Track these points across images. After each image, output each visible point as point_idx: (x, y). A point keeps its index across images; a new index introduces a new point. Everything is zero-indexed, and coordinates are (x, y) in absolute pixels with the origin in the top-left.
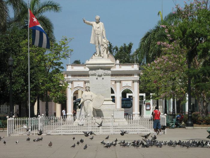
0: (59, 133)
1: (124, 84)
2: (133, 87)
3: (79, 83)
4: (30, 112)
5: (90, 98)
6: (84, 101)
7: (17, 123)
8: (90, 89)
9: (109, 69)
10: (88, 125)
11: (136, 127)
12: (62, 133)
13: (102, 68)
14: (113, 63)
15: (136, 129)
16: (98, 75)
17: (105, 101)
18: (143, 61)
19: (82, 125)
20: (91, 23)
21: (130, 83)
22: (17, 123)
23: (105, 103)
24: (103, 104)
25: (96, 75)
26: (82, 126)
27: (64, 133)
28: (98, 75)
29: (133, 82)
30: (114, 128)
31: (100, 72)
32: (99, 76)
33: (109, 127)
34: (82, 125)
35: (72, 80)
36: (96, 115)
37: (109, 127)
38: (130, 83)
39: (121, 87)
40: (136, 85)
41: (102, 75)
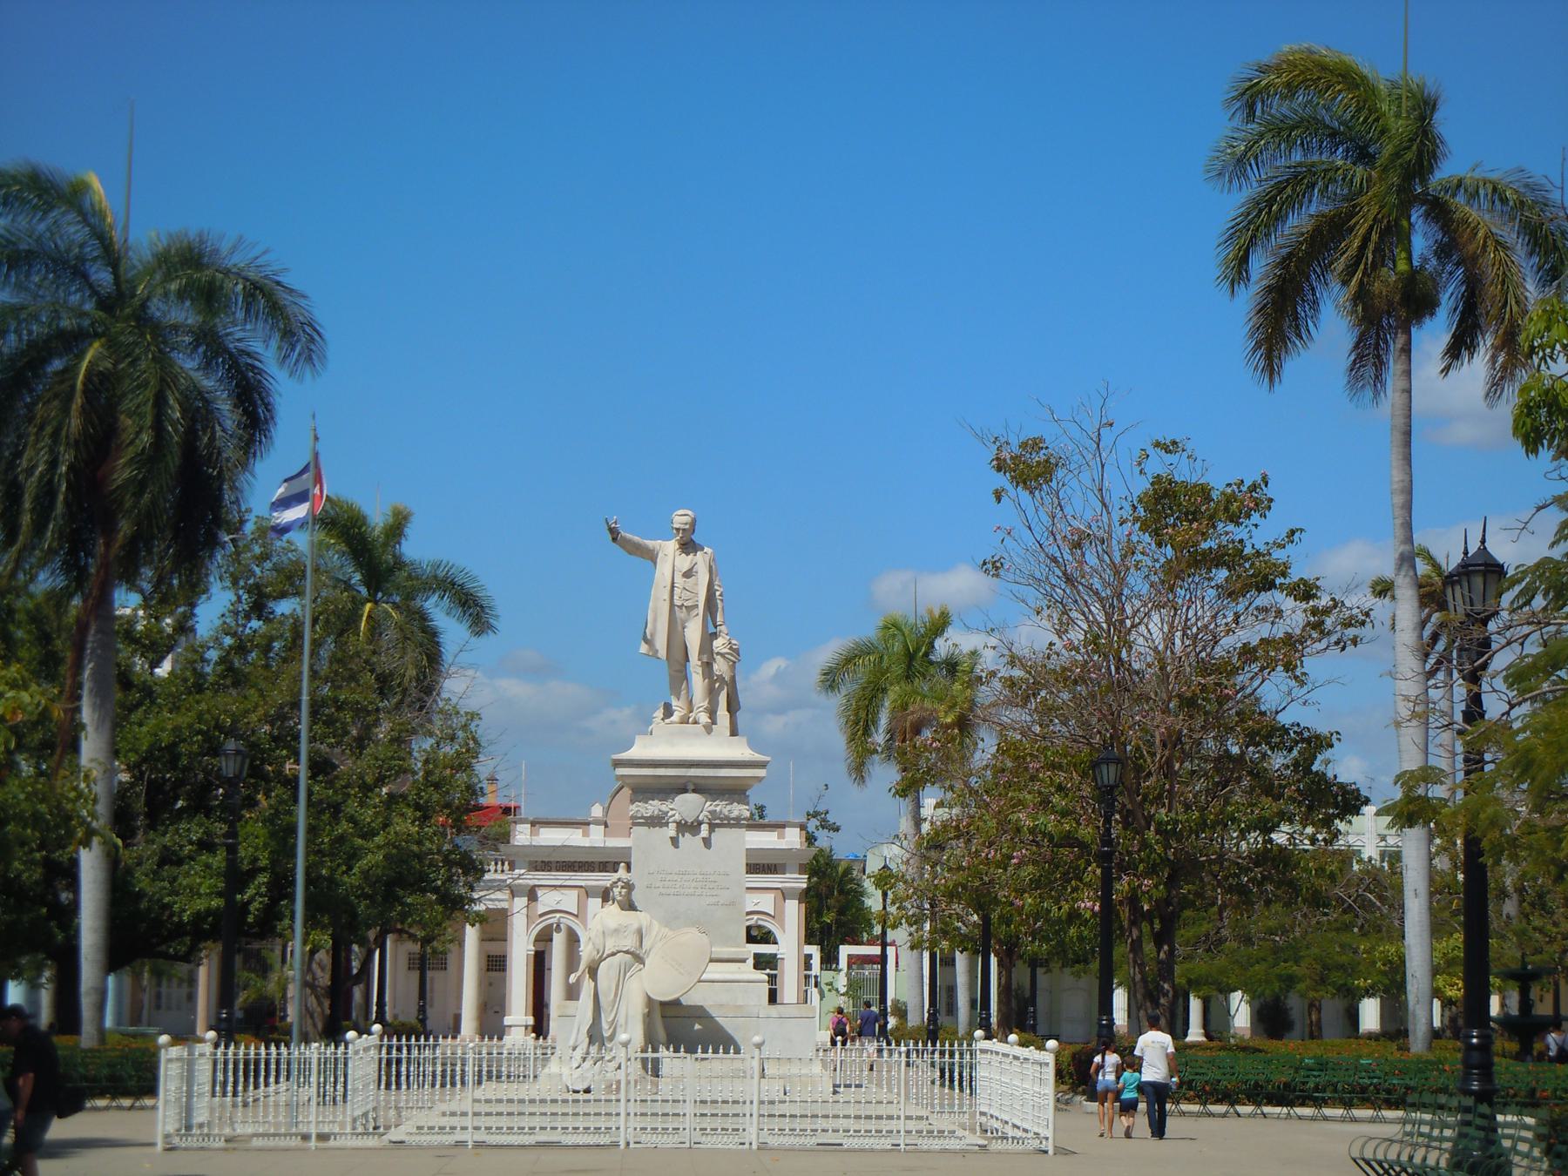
0: (459, 1136)
2: (777, 916)
3: (558, 896)
4: (1000, 1002)
6: (601, 960)
7: (273, 1066)
8: (636, 896)
9: (735, 791)
10: (618, 1089)
11: (882, 1110)
12: (469, 1137)
13: (700, 788)
14: (758, 757)
15: (880, 1113)
16: (679, 824)
17: (712, 961)
18: (1501, 359)
19: (587, 1091)
20: (650, 543)
22: (273, 1066)
23: (716, 971)
24: (704, 977)
25: (667, 824)
26: (587, 1096)
27: (481, 1136)
28: (679, 824)
29: (785, 894)
30: (765, 1110)
31: (687, 805)
32: (683, 827)
33: (738, 1109)
34: (587, 1091)
35: (532, 883)
36: (661, 1034)
37: (738, 1109)
38: (766, 902)
40: (793, 911)
41: (700, 823)
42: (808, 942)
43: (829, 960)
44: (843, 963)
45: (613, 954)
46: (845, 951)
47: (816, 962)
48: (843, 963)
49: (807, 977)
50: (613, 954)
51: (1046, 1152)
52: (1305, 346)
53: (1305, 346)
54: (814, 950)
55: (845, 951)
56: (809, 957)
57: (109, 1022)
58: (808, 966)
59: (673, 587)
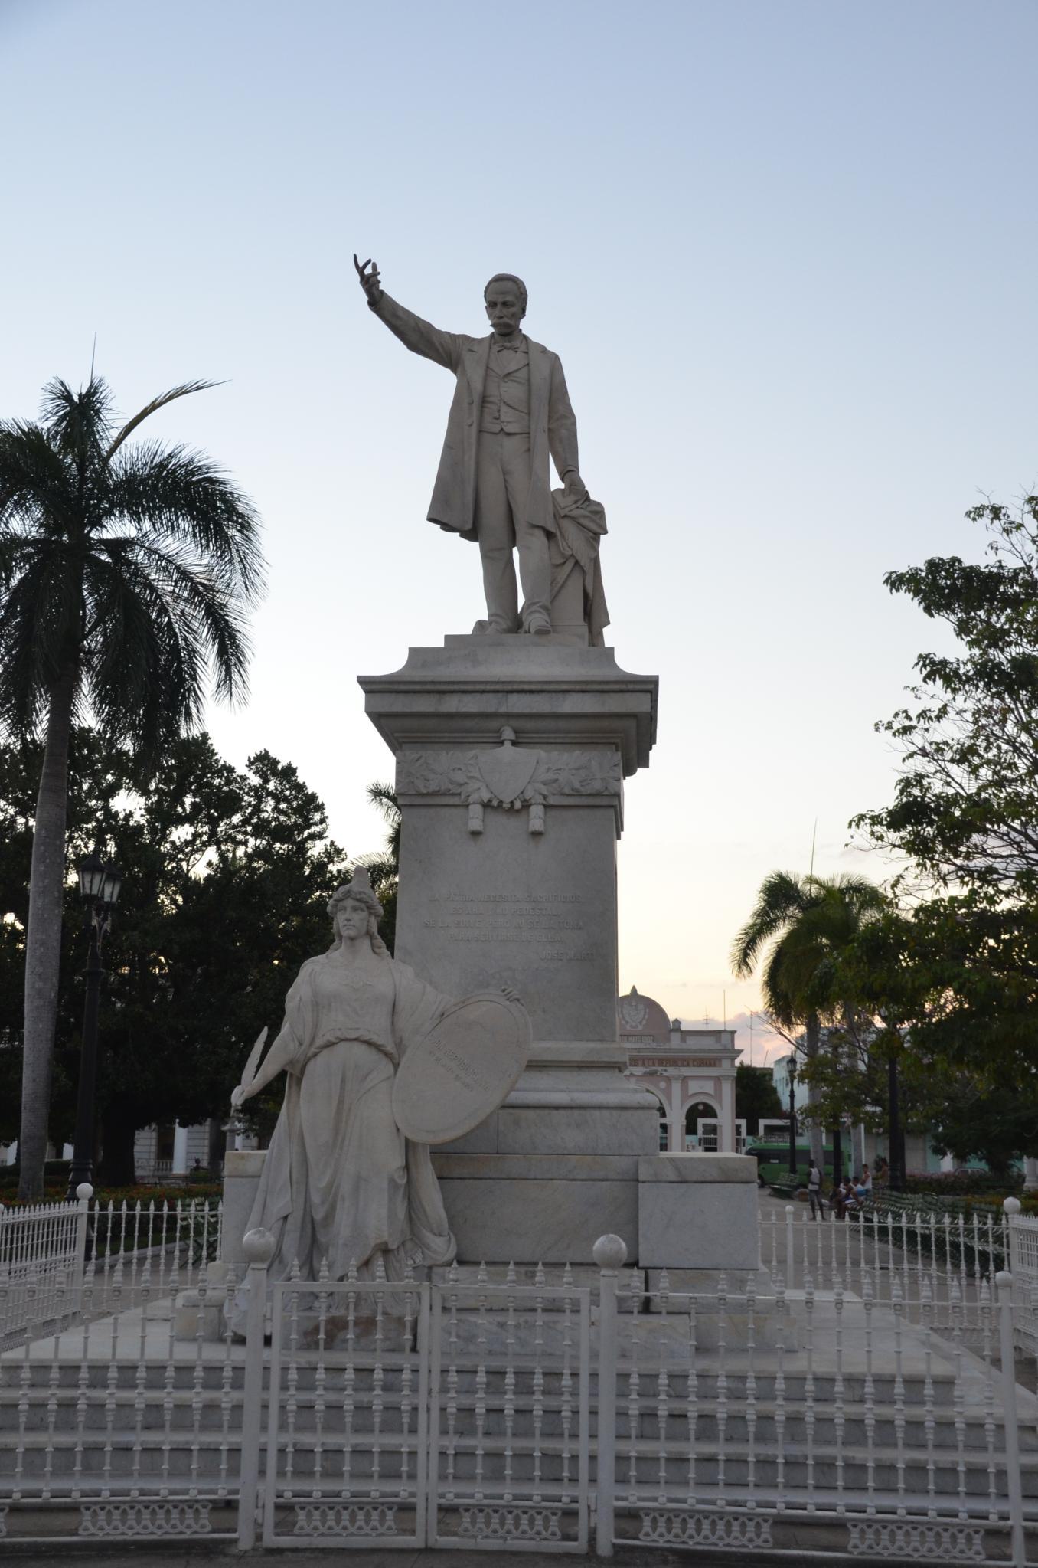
1: (694, 1087)
2: (718, 1095)
5: (376, 1026)
21: (709, 1087)
24: (515, 1097)
38: (709, 1087)
39: (685, 1095)
41: (526, 805)
42: (738, 1116)
43: (752, 1130)
44: (700, 1129)
45: (329, 1045)
46: (762, 1123)
47: (744, 1130)
48: (761, 1131)
49: (738, 1140)
50: (329, 1045)
51: (664, 1147)
52: (263, 598)
53: (263, 598)
54: (743, 1122)
55: (762, 1123)
56: (738, 1127)
57: (265, 1032)
58: (738, 1133)
59: (343, 1081)
